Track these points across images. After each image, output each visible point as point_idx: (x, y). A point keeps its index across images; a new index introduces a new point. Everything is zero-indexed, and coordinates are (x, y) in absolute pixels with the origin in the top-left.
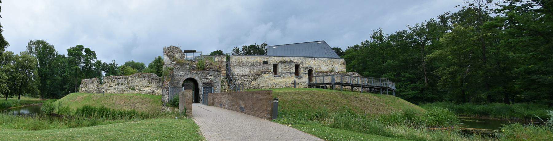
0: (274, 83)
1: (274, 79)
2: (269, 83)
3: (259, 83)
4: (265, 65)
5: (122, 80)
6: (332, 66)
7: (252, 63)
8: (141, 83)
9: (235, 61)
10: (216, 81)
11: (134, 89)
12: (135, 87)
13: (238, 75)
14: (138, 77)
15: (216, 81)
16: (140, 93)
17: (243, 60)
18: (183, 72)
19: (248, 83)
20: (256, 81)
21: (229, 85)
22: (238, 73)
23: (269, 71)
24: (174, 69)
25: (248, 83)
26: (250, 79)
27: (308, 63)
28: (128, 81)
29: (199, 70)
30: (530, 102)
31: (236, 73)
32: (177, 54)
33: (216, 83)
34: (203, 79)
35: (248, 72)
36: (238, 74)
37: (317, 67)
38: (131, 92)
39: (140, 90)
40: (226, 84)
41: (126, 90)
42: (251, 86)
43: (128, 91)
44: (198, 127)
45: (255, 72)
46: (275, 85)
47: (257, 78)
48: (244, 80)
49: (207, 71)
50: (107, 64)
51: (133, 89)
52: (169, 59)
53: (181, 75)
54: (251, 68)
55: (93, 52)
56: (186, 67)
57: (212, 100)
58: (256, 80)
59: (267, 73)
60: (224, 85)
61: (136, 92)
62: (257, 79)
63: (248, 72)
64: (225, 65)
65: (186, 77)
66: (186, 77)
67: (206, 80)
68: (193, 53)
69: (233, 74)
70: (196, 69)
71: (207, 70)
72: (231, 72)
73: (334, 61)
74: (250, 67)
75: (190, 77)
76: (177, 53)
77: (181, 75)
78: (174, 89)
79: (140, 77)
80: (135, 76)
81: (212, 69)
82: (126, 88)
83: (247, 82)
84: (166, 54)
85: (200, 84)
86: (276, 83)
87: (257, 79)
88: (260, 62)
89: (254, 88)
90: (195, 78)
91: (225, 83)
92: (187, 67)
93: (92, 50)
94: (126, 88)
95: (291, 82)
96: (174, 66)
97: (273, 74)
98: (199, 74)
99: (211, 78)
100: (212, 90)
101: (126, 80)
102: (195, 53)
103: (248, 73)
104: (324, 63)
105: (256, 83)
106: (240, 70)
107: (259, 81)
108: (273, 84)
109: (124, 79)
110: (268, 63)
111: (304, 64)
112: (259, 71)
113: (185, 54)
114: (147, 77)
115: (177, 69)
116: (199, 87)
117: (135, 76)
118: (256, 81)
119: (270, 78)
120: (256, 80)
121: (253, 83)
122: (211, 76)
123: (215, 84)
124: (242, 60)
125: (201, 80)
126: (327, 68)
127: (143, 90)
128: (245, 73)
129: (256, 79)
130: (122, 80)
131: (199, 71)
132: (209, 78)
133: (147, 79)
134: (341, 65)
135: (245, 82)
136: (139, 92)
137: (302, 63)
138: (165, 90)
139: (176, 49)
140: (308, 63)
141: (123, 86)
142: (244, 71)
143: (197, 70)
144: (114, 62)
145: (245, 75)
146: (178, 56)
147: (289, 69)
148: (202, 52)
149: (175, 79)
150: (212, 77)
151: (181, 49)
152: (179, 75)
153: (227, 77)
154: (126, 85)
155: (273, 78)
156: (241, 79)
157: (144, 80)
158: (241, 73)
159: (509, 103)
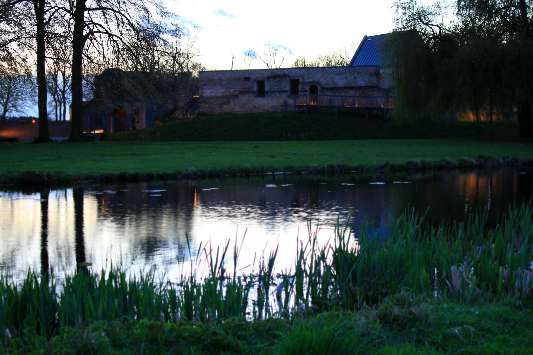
4: (247, 82)
6: (355, 78)
30: (348, 310)
37: (328, 81)
44: (47, 241)
111: (305, 78)
126: (346, 81)
147: (279, 86)
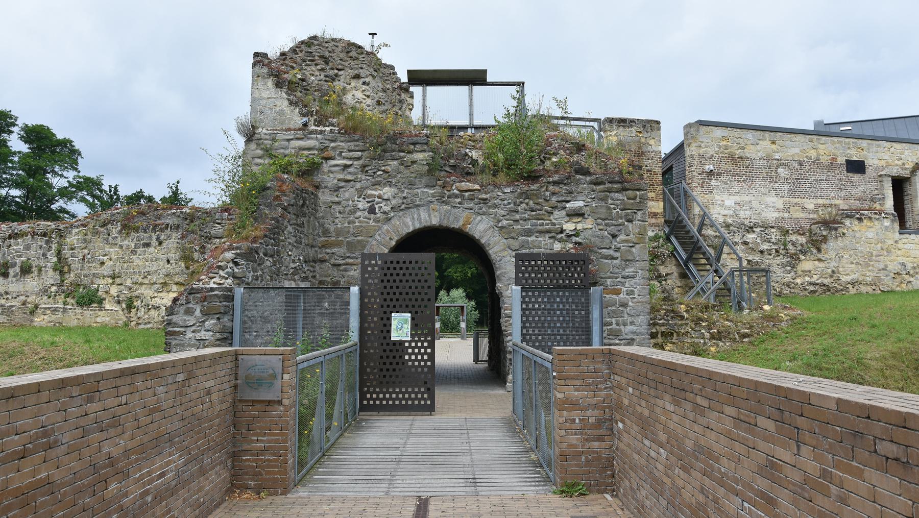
1: (900, 245)
2: (881, 266)
3: (833, 264)
4: (856, 177)
5: (28, 248)
8: (137, 261)
9: (711, 151)
10: (617, 250)
11: (91, 302)
12: (102, 284)
13: (728, 226)
14: (124, 227)
15: (617, 250)
16: (126, 325)
17: (751, 151)
18: (387, 192)
19: (784, 266)
20: (820, 256)
21: (683, 276)
22: (726, 212)
23: (878, 207)
24: (325, 167)
25: (784, 266)
26: (790, 247)
28: (66, 252)
29: (502, 178)
31: (717, 214)
32: (354, 83)
33: (613, 258)
34: (529, 233)
35: (778, 210)
36: (730, 221)
38: (76, 316)
39: (130, 307)
40: (669, 269)
41: (45, 302)
42: (799, 281)
43: (55, 310)
45: (810, 212)
46: (908, 273)
47: (825, 239)
48: (762, 252)
49: (554, 183)
50: (150, 199)
51: (90, 300)
52: (291, 103)
53: (372, 211)
54: (793, 193)
55: (66, 143)
56: (409, 158)
57: (599, 423)
58: (819, 250)
59: (870, 218)
60: (660, 276)
61: (103, 318)
62: (824, 246)
63: (778, 210)
64: (659, 170)
65: (410, 223)
66: (408, 220)
67: (544, 240)
68: (465, 89)
69: (704, 216)
70: (482, 172)
71: (556, 178)
72: (688, 210)
74: (786, 187)
75: (435, 221)
76: (357, 77)
77: (372, 211)
78: (320, 300)
79: (136, 229)
80: (104, 225)
81: (585, 172)
82: (45, 291)
83: (778, 260)
84: (271, 74)
85: (506, 267)
86: (909, 266)
87: (824, 246)
88: (832, 165)
89: (812, 288)
90: (468, 229)
91: (663, 263)
92: (419, 156)
93: (60, 136)
94: (45, 291)
96: (324, 149)
97: (893, 221)
98: (496, 206)
99: (580, 226)
100: (588, 313)
101: (54, 246)
102: (477, 89)
103: (776, 215)
105: (821, 265)
106: (737, 198)
107: (832, 254)
108: (898, 268)
109: (41, 242)
110: (869, 171)
112: (831, 205)
113: (416, 90)
114: (177, 227)
115: (346, 167)
116: (499, 284)
117: (104, 225)
118: (820, 256)
119: (883, 242)
120: (819, 250)
121: (806, 265)
122: (577, 214)
123: (605, 267)
124: (743, 148)
127: (148, 308)
128: (764, 215)
129: (817, 243)
130: (28, 248)
131: (498, 186)
132: (569, 227)
133: (172, 241)
135: (768, 261)
136: (122, 317)
138: (189, 312)
139: (353, 54)
141: (31, 284)
143: (486, 178)
144: (177, 189)
145: (766, 227)
146: (359, 95)
148: (522, 84)
149: (326, 232)
150: (588, 223)
151: (385, 57)
152: (355, 209)
153: (671, 233)
154: (50, 277)
155: (896, 242)
156: (746, 243)
157: (154, 242)
158: (742, 214)
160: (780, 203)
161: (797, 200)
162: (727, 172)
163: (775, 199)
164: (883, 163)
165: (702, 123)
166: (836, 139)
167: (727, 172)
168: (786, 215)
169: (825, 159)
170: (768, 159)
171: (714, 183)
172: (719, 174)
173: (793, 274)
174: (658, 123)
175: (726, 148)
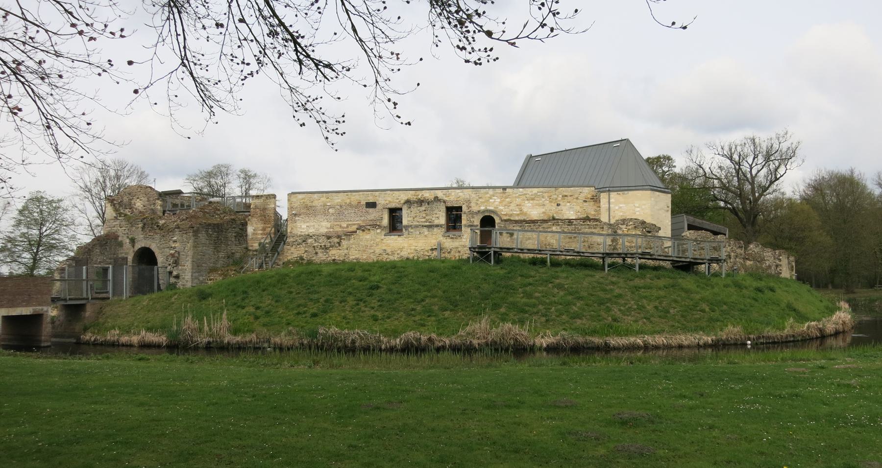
0: (385, 250)
1: (384, 241)
2: (372, 251)
4: (371, 210)
7: (339, 207)
17: (316, 203)
20: (340, 248)
27: (484, 202)
35: (328, 228)
63: (328, 228)
73: (565, 194)
74: (332, 218)
76: (138, 198)
95: (430, 248)
103: (326, 230)
104: (533, 199)
110: (379, 207)
111: (472, 204)
122: (175, 241)
125: (161, 251)
128: (320, 230)
134: (585, 201)
137: (469, 201)
140: (484, 202)
142: (316, 226)
147: (427, 218)
159: (479, 344)
160: (329, 225)
161: (337, 223)
162: (304, 213)
163: (326, 223)
164: (387, 202)
165: (293, 193)
166: (361, 193)
167: (304, 213)
168: (332, 230)
169: (354, 203)
170: (325, 205)
171: (297, 218)
172: (300, 215)
173: (327, 256)
174: (274, 196)
175: (304, 202)
